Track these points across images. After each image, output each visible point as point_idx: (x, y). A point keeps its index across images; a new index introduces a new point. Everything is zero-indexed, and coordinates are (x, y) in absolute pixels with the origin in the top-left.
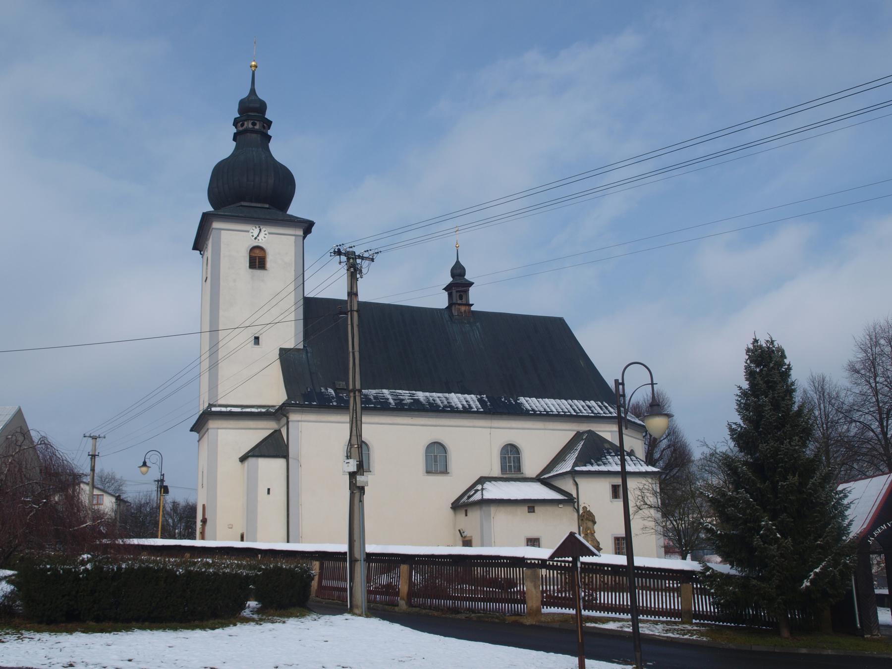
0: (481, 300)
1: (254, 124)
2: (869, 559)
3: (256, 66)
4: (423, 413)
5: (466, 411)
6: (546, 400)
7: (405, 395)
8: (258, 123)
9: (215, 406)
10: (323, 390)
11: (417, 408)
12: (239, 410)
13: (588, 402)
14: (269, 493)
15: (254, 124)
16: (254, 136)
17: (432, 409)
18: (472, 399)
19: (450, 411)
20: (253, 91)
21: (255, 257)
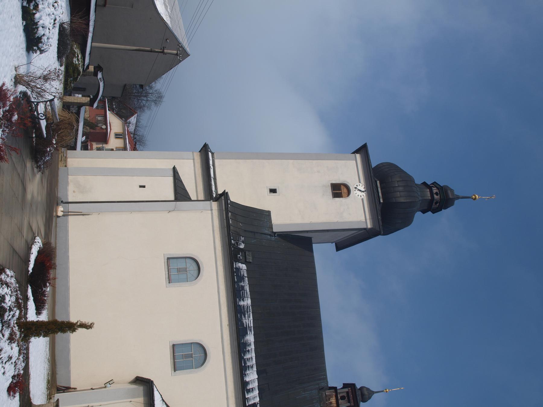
1: (437, 194)
2: (33, 323)
3: (475, 199)
4: (235, 336)
7: (249, 321)
8: (439, 197)
9: (213, 157)
10: (243, 239)
11: (238, 331)
12: (212, 175)
14: (141, 187)
15: (437, 194)
16: (429, 194)
17: (240, 349)
19: (241, 369)
20: (458, 198)
21: (340, 190)
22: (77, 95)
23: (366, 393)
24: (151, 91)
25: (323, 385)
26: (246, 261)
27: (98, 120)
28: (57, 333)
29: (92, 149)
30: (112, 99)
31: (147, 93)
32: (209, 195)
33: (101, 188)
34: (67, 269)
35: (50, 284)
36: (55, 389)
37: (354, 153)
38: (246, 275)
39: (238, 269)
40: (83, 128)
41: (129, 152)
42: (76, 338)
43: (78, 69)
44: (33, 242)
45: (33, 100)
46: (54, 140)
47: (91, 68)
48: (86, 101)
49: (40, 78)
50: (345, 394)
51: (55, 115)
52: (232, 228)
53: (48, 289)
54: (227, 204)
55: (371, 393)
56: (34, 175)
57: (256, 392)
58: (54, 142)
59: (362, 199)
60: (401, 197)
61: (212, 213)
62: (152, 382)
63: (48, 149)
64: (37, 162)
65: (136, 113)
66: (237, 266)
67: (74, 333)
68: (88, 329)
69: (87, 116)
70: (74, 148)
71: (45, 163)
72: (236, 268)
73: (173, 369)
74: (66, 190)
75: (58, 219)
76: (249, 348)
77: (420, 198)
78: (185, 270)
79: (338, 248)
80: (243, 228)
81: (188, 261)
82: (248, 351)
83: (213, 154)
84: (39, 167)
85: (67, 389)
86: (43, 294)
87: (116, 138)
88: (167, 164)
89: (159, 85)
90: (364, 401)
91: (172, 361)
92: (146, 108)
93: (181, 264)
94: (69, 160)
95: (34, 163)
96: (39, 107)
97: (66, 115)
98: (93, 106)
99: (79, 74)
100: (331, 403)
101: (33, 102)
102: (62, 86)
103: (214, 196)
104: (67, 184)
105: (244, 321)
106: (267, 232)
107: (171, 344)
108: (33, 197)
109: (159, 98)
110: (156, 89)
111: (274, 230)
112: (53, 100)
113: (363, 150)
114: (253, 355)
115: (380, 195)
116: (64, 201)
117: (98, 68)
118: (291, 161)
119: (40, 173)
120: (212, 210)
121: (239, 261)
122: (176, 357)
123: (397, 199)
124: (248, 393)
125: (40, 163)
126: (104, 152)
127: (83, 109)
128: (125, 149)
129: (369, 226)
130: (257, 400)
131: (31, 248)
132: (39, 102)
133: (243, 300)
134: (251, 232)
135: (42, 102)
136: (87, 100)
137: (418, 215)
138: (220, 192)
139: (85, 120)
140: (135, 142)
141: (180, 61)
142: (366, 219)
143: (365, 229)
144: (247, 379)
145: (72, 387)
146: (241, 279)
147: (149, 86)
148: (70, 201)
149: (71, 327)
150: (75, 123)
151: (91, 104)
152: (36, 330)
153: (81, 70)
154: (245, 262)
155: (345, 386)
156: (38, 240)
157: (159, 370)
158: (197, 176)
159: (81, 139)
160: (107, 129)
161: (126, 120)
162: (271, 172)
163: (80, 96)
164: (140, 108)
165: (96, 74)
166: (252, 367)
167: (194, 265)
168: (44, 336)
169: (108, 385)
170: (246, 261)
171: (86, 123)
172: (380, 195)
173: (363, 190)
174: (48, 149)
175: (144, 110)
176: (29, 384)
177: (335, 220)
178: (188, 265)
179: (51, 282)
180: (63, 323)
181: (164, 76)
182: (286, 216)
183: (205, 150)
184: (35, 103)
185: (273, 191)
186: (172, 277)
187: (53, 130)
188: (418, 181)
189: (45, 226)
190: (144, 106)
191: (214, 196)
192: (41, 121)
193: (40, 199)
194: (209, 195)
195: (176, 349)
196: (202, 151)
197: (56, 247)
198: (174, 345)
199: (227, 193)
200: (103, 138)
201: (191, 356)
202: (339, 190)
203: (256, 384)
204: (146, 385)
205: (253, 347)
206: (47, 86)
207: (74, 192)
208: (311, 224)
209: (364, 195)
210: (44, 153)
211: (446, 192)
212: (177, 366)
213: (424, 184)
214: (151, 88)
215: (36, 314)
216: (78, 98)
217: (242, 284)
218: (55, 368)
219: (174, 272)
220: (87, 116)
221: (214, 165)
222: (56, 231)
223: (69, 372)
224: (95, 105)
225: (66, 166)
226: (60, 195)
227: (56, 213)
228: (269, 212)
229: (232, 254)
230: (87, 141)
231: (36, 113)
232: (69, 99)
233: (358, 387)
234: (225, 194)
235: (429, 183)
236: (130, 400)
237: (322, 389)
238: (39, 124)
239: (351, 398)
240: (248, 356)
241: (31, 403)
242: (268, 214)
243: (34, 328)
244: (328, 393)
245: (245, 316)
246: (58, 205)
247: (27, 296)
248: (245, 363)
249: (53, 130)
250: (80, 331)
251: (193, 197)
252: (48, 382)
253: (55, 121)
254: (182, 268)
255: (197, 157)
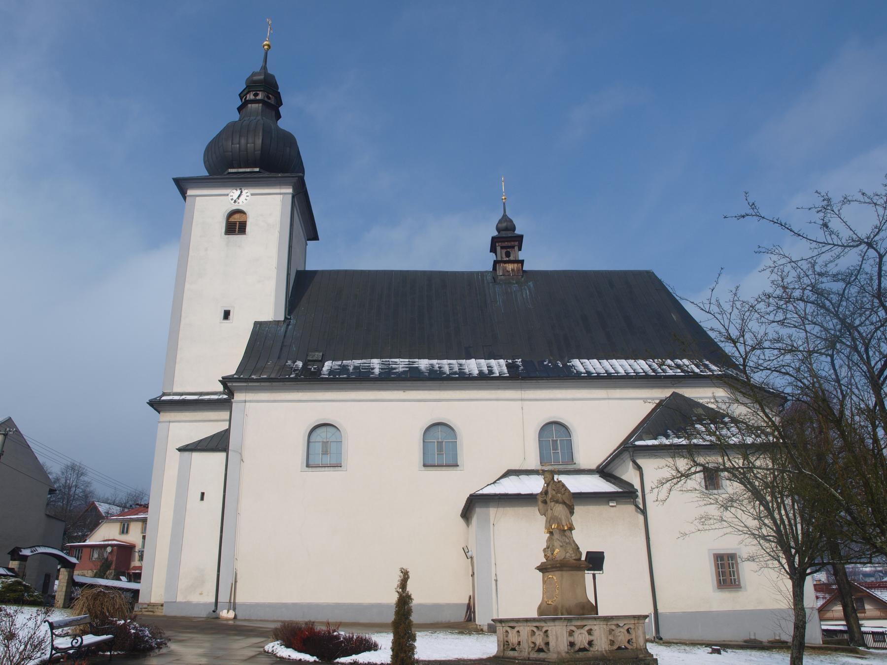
0: (537, 257)
1: (256, 95)
2: (395, 656)
3: (269, 46)
4: (419, 383)
5: (485, 379)
6: (614, 361)
7: (401, 364)
9: (169, 394)
10: (289, 362)
11: (413, 378)
13: (679, 361)
15: (256, 95)
16: (255, 106)
17: (436, 378)
18: (499, 366)
19: (462, 379)
20: (264, 68)
21: (235, 223)
22: (56, 587)
23: (504, 225)
24: (63, 481)
25: (489, 278)
26: (320, 361)
27: (99, 558)
28: (411, 621)
29: (140, 568)
30: (68, 536)
31: (64, 487)
32: (224, 404)
33: (199, 555)
34: (310, 606)
35: (334, 631)
36: (469, 623)
37: (185, 198)
38: (339, 363)
39: (331, 371)
40: (107, 578)
41: (150, 515)
42: (419, 596)
43: (10, 585)
44: (273, 655)
45: (48, 656)
46: (119, 622)
47: (14, 564)
48: (66, 573)
49: (8, 647)
50: (504, 251)
51: (77, 620)
52: (273, 376)
53: (342, 633)
54: (239, 380)
55: (505, 218)
56: (171, 653)
57: (493, 362)
58: (122, 622)
59: (252, 195)
60: (255, 143)
61: (250, 401)
62: (471, 495)
63: (133, 631)
64: (151, 649)
65: (93, 503)
66: (326, 373)
67: (413, 597)
68: (408, 577)
69: (90, 573)
70: (136, 593)
71: (154, 636)
72: (329, 374)
73: (455, 468)
74: (197, 605)
75: (238, 617)
76: (436, 367)
77: (259, 118)
78: (325, 444)
79: (315, 237)
80: (277, 359)
81: (313, 439)
82: (440, 368)
83: (164, 394)
84: (159, 646)
85: (470, 609)
86: (349, 640)
87: (127, 532)
88: (173, 458)
89: (54, 468)
90: (514, 229)
91: (444, 468)
92: (88, 489)
93: (317, 448)
94: (153, 600)
95: (152, 654)
96: (60, 646)
97: (79, 604)
98: (75, 564)
99: (20, 583)
100: (513, 270)
101: (51, 655)
102: (26, 609)
103: (225, 397)
104: (188, 604)
105: (401, 370)
106: (283, 329)
107: (423, 468)
108: (204, 655)
109: (75, 470)
110: (60, 473)
111: (282, 319)
112: (52, 626)
113: (182, 185)
114: (445, 362)
115: (248, 170)
116: (213, 608)
117: (15, 554)
118: (187, 286)
119: (169, 644)
120: (245, 401)
121: (319, 370)
122: (440, 463)
123: (257, 148)
124: (493, 373)
125: (154, 645)
126: (145, 550)
127: (78, 579)
128: (144, 521)
129: (290, 190)
130: (502, 362)
131: (282, 658)
132: (52, 645)
133: (373, 369)
134: (281, 349)
135: (52, 641)
136: (64, 573)
137: (282, 124)
138: (220, 388)
139: (96, 576)
140: (136, 507)
141: (17, 431)
142: (280, 194)
143: (293, 197)
144: (476, 372)
145: (467, 602)
146: (344, 369)
147: (55, 482)
148: (214, 600)
149: (404, 600)
150: (94, 591)
151: (71, 566)
152: (405, 652)
153: (13, 579)
154: (322, 362)
155: (493, 249)
156: (269, 647)
157: (457, 486)
158: (194, 419)
159: (124, 583)
160: (112, 546)
161: (103, 518)
162: (200, 315)
163: (57, 582)
164: (86, 496)
165: (25, 558)
166: (461, 365)
167: (319, 431)
168: (414, 640)
169: (469, 554)
170: (320, 361)
171: (101, 574)
172: (248, 170)
173: (239, 192)
174: (133, 631)
175: (90, 492)
176: (470, 660)
177: (277, 235)
178: (319, 439)
179: (332, 628)
180: (397, 613)
181: (41, 459)
182: (266, 302)
183: (158, 405)
184: (54, 652)
185: (227, 315)
186: (334, 462)
187: (103, 624)
188: (236, 117)
189: (248, 636)
190: (84, 491)
191: (225, 397)
192: (85, 643)
193: (207, 645)
194: (224, 404)
195: (430, 462)
196: (159, 409)
197: (282, 622)
198: (425, 465)
199: (223, 378)
200: (126, 551)
201: (440, 444)
202: (236, 225)
203: (483, 362)
204: (474, 504)
205: (435, 362)
206: (23, 634)
207: (201, 594)
208: (278, 268)
209: (246, 192)
210: (138, 638)
211: (255, 82)
212: (451, 463)
213: (240, 109)
214: (57, 480)
215: (376, 650)
216: (59, 586)
217: (351, 368)
218: (442, 623)
219: (327, 460)
220: (90, 573)
221: (181, 394)
222: (256, 620)
223: (448, 605)
224: (73, 560)
225: (162, 605)
226: (203, 614)
227: (228, 620)
228: (256, 323)
229: (310, 378)
230: (129, 574)
231: (71, 652)
232: (60, 597)
233: (495, 233)
234: (225, 381)
235: (239, 103)
236: (492, 526)
237: (494, 279)
238: (89, 646)
239: (509, 244)
240: (446, 369)
241: (495, 657)
242: (259, 326)
243: (403, 655)
244: (500, 272)
245: (395, 369)
246: (218, 618)
247: (351, 663)
248: (455, 373)
249: (103, 624)
250: (410, 588)
251: (224, 426)
252: (461, 633)
253: (88, 620)
254: (323, 447)
255: (166, 416)
